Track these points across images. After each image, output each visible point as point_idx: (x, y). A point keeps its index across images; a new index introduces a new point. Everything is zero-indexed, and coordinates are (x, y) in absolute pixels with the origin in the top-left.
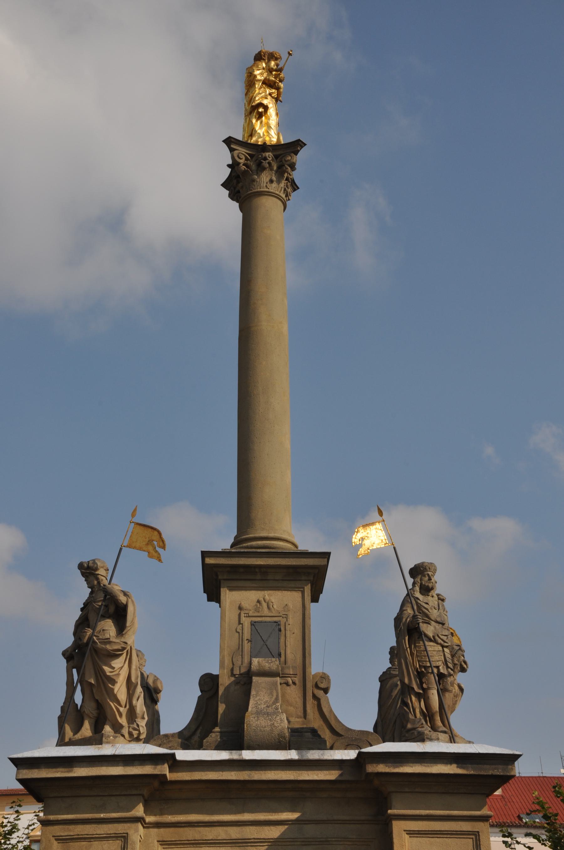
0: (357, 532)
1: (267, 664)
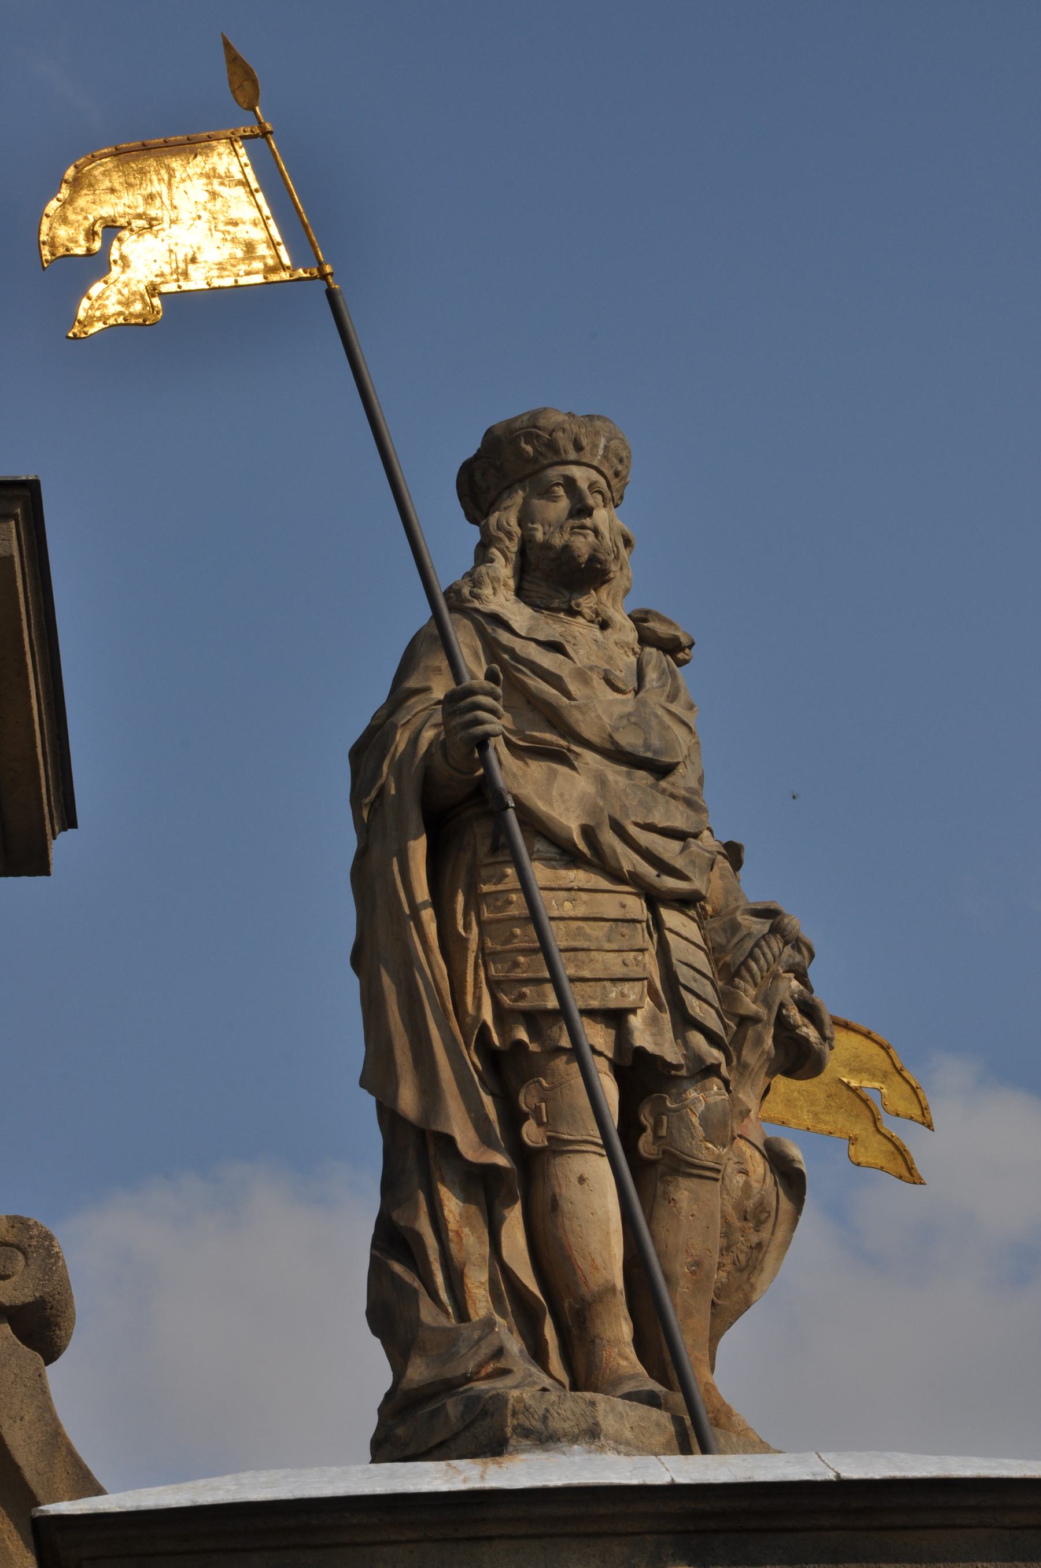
0: (76, 184)
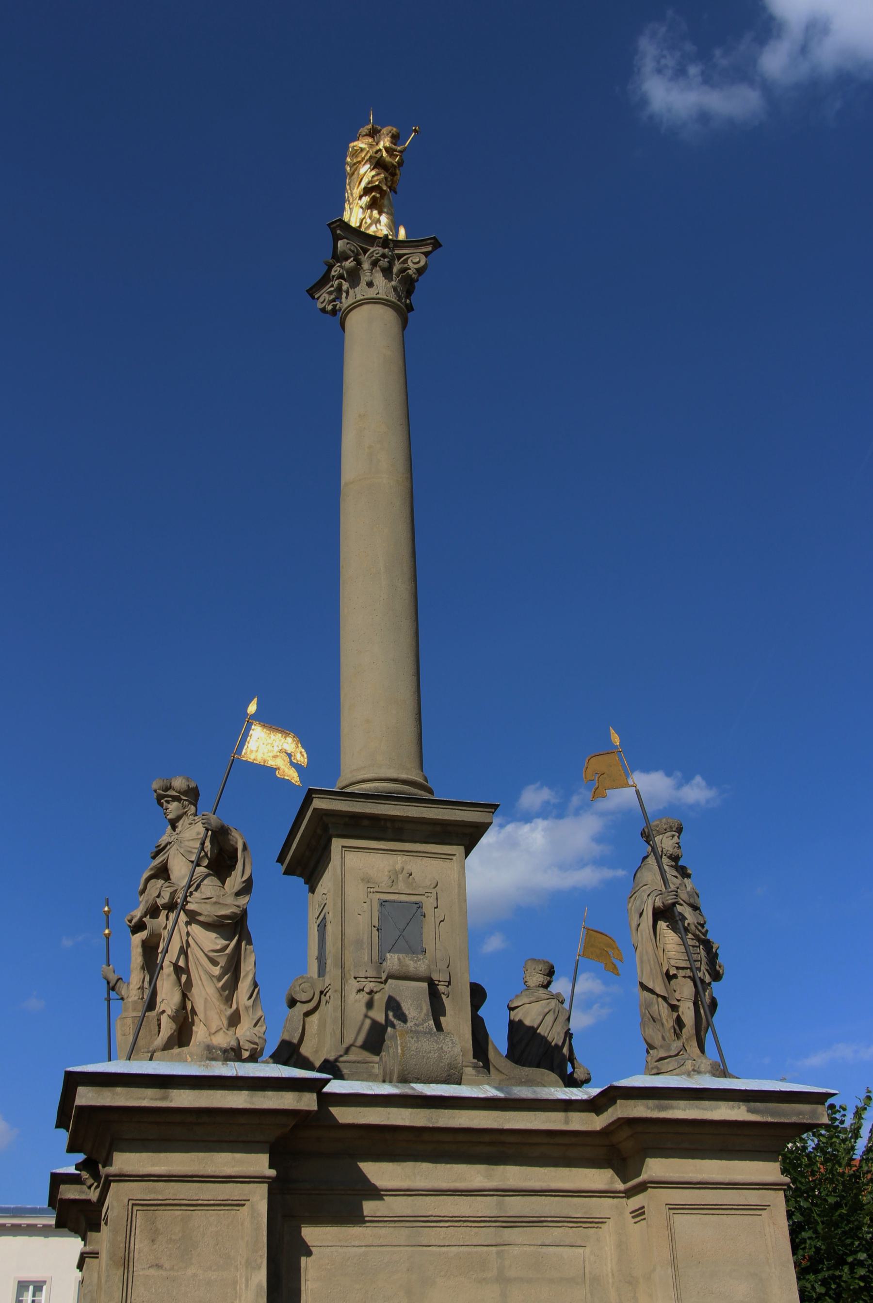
1: (412, 962)
